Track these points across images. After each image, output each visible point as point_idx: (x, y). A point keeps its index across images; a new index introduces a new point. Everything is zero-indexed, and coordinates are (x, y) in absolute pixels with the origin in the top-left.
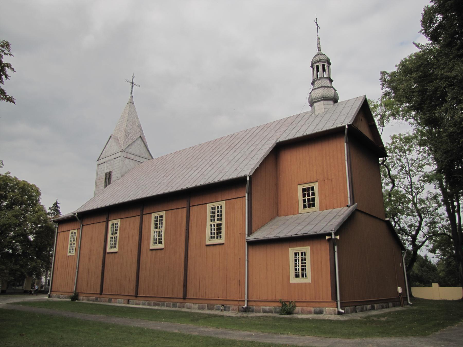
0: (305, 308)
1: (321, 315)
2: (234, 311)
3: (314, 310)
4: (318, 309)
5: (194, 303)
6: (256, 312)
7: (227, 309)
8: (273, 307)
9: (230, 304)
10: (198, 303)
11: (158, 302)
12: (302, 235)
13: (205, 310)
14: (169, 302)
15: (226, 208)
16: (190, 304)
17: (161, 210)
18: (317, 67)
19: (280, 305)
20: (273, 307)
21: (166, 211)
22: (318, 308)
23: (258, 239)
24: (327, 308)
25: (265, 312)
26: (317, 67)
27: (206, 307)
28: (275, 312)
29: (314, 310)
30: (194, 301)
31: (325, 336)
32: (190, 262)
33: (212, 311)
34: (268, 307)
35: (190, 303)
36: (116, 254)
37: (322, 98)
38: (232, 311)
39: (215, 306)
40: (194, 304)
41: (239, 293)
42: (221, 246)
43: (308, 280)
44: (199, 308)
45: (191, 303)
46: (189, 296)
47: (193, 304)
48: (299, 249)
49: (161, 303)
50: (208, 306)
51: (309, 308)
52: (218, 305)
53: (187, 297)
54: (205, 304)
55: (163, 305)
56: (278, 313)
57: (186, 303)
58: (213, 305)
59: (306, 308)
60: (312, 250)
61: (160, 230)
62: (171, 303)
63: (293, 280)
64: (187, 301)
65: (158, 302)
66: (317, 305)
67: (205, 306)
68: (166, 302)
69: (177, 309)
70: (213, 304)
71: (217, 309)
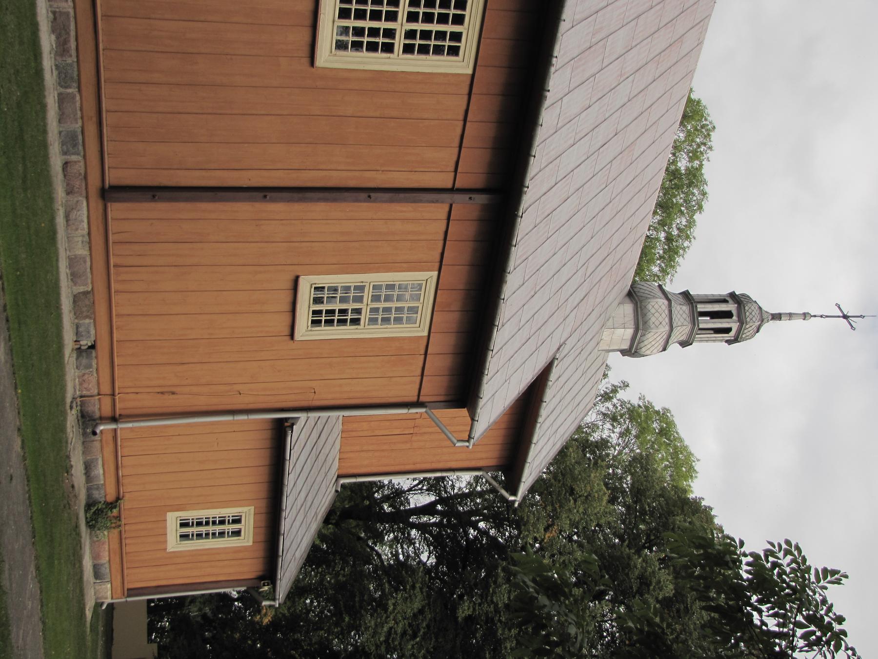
0: (107, 547)
1: (92, 579)
2: (81, 384)
3: (105, 564)
4: (105, 570)
5: (89, 234)
6: (83, 443)
7: (84, 361)
8: (102, 482)
9: (100, 369)
10: (91, 255)
11: (73, 44)
12: (281, 554)
13: (70, 283)
14: (81, 110)
15: (404, 339)
16: (85, 225)
17: (438, 299)
18: (728, 315)
19: (111, 498)
20: (102, 482)
21: (473, 76)
22: (108, 570)
23: (287, 463)
24: (109, 586)
25: (88, 467)
26: (728, 315)
27: (82, 289)
28: (89, 489)
29: (102, 565)
30: (98, 240)
31: (8, 307)
32: (244, 209)
33: (72, 315)
34: (101, 472)
35: (88, 217)
36: (306, 61)
37: (636, 349)
38: (79, 377)
39: (87, 321)
40: (86, 238)
41: (137, 393)
42: (305, 51)
43: (173, 544)
44: (73, 261)
45: (89, 228)
46: (116, 209)
47: (86, 231)
48: (248, 526)
49: (71, 59)
50: (86, 293)
51: (75, 54)
52: (93, 332)
53: (109, 204)
54: (92, 283)
55: (64, 79)
56: (89, 496)
57: (87, 198)
58: (93, 315)
59: (107, 549)
60: (245, 549)
61: (396, 42)
62: (80, 123)
63: (172, 519)
64: (96, 203)
65: (73, 44)
66: (116, 566)
67: (86, 285)
68: (80, 91)
69: (56, 161)
70: (94, 313)
71: (80, 330)
